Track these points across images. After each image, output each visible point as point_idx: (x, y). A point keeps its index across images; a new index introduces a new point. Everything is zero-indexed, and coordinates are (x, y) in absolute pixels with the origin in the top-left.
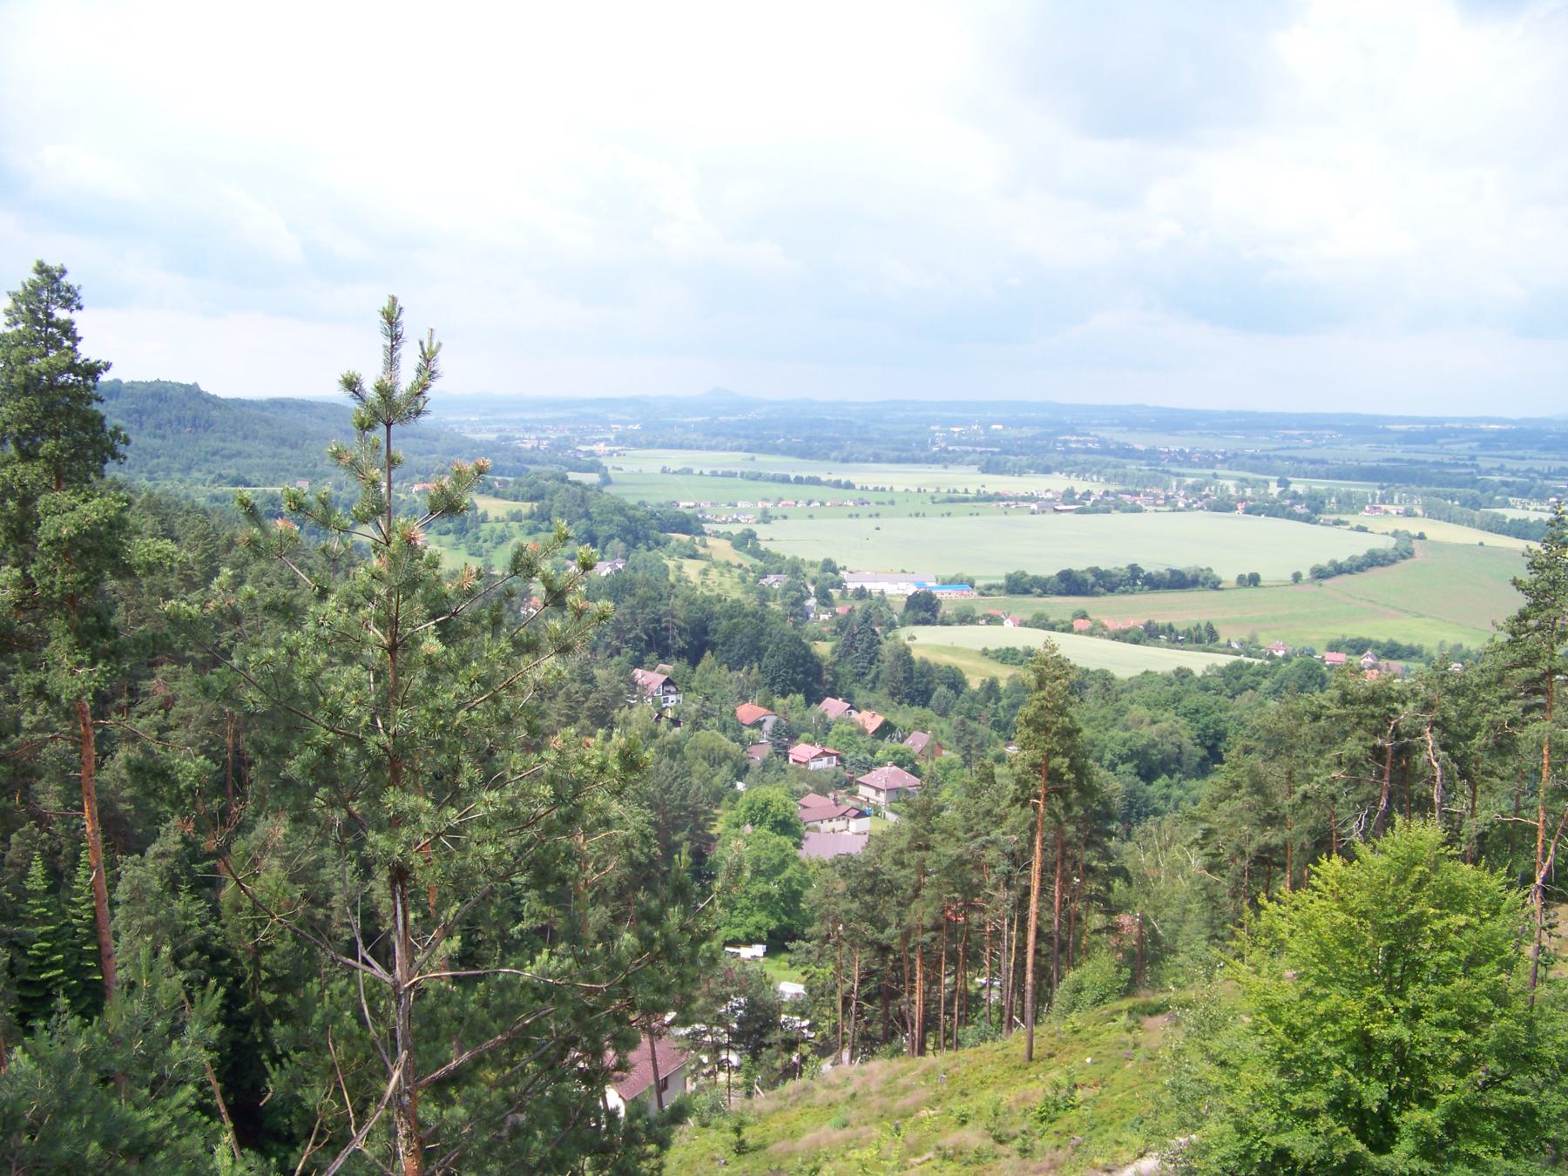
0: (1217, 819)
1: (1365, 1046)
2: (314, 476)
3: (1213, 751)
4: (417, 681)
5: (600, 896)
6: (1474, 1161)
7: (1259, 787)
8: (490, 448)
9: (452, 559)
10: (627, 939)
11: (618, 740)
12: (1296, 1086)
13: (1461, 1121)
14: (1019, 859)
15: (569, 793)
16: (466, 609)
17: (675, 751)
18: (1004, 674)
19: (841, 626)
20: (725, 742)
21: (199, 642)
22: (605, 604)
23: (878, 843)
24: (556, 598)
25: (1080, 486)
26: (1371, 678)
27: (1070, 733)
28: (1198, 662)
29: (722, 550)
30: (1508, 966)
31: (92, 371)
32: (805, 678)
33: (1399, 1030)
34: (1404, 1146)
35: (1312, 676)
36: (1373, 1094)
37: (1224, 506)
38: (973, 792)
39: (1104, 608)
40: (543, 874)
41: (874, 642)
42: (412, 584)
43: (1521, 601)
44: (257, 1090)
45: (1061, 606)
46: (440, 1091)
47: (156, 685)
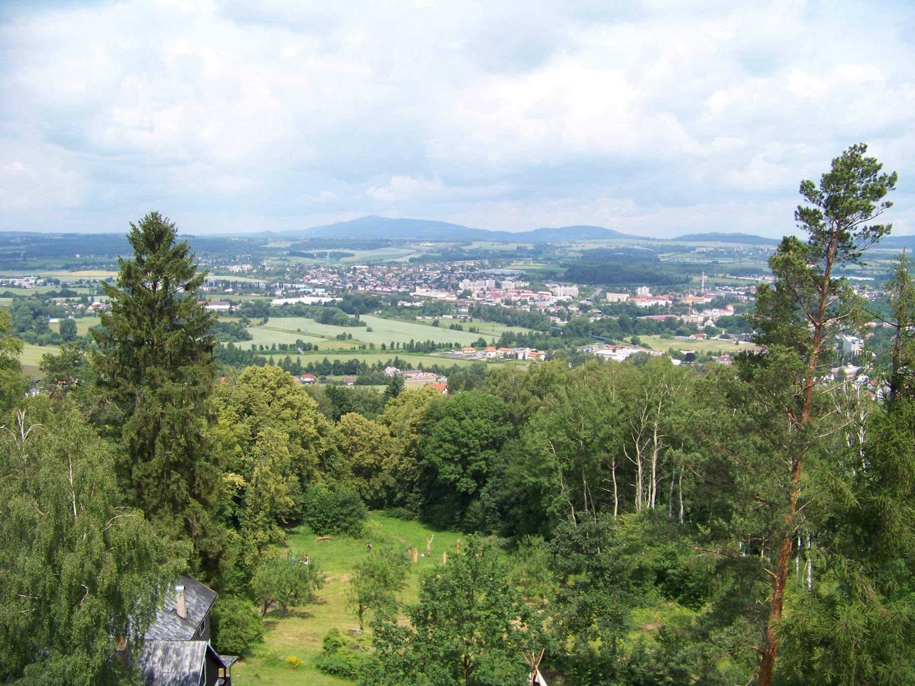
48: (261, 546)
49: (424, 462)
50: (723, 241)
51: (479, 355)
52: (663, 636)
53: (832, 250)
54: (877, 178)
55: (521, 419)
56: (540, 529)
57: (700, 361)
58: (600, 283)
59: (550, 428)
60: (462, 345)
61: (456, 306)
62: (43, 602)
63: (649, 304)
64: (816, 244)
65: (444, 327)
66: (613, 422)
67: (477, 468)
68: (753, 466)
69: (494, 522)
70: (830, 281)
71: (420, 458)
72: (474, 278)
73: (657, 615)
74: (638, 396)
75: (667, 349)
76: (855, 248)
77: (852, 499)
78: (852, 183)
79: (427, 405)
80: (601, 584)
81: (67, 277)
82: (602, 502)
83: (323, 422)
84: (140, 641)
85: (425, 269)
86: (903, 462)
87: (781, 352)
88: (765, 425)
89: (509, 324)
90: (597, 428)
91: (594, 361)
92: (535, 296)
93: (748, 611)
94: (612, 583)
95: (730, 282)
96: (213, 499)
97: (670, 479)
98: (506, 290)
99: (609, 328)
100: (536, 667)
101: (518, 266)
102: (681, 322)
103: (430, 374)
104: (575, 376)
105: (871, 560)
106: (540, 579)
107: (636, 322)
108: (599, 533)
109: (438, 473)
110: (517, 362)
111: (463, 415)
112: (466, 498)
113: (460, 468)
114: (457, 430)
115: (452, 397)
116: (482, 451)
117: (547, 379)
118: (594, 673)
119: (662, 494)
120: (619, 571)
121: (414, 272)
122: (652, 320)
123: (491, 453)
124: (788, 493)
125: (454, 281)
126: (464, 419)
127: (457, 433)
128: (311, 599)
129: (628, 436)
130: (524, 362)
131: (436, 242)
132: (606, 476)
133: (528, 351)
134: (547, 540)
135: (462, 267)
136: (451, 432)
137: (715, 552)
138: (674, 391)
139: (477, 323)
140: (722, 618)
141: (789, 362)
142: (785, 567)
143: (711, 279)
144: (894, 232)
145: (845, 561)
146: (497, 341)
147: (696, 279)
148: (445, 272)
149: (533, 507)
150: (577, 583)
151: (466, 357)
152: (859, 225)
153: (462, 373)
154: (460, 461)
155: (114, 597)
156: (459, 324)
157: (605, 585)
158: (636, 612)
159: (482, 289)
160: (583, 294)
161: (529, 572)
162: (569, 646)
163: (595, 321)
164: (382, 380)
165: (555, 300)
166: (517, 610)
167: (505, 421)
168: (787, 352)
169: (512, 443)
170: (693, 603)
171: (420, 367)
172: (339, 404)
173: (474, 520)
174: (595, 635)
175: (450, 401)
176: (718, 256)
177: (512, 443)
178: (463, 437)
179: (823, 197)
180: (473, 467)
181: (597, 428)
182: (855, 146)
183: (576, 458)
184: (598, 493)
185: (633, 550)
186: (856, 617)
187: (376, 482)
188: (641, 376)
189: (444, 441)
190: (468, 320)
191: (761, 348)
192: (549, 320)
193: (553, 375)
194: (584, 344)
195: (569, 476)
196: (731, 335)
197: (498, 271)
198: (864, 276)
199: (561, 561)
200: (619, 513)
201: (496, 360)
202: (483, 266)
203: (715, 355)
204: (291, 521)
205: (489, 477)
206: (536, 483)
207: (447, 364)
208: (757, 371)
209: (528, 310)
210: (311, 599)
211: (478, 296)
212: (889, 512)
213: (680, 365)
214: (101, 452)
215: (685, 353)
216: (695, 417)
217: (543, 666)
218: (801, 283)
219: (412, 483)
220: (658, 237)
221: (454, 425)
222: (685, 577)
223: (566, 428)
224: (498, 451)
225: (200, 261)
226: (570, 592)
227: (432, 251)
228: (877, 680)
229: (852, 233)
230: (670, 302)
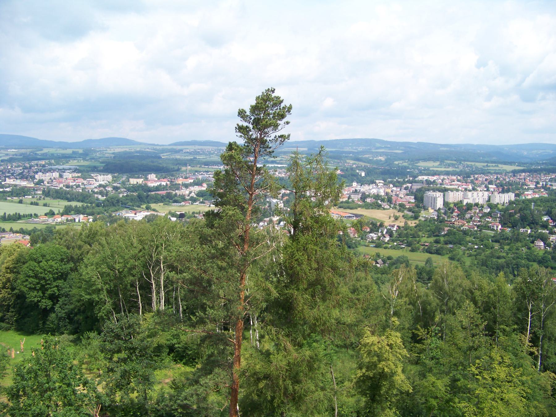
49: (16, 291)
50: (199, 145)
51: (50, 220)
52: (175, 385)
53: (257, 150)
54: (281, 107)
55: (79, 259)
56: (95, 327)
57: (188, 218)
58: (124, 173)
59: (97, 264)
60: (39, 215)
61: (34, 190)
63: (156, 184)
64: (248, 146)
65: (26, 203)
66: (135, 257)
67: (52, 293)
68: (217, 279)
69: (65, 326)
70: (257, 168)
71: (13, 289)
72: (45, 172)
73: (170, 373)
74: (150, 241)
75: (168, 212)
76: (270, 148)
77: (275, 294)
78: (267, 110)
79: (16, 254)
80: (134, 358)
82: (132, 307)
85: (12, 167)
86: (301, 270)
87: (230, 210)
88: (223, 254)
89: (69, 200)
90: (126, 262)
91: (123, 220)
92: (85, 182)
93: (221, 365)
94: (141, 356)
95: (204, 170)
97: (173, 290)
98: (66, 179)
99: (132, 200)
100: (97, 414)
101: (74, 163)
102: (176, 194)
103: (18, 235)
104: (111, 230)
105: (288, 328)
106: (97, 359)
107: (148, 196)
108: (130, 326)
109: (26, 298)
110: (75, 224)
111: (41, 259)
112: (46, 312)
113: (40, 293)
114: (37, 269)
115: (33, 248)
116: (54, 281)
117: (94, 233)
118: (134, 413)
119: (169, 299)
120: (145, 349)
121: (4, 169)
122: (158, 194)
123: (60, 282)
124: (238, 293)
125: (32, 174)
126: (41, 262)
127: (38, 271)
129: (145, 266)
130: (79, 224)
131: (18, 149)
132: (133, 291)
133: (82, 216)
134: (99, 334)
135: (37, 165)
136: (33, 271)
137: (199, 332)
138: (171, 237)
139: (48, 200)
140: (206, 370)
141: (234, 216)
142: (240, 337)
143: (193, 168)
144: (292, 139)
145: (274, 330)
146: (61, 211)
147: (184, 168)
148: (25, 168)
149: (89, 314)
150: (119, 358)
151: (42, 222)
152: (272, 135)
153: (39, 232)
154: (40, 289)
156: (36, 201)
157: (137, 358)
158: (157, 372)
159: (51, 179)
160: (115, 179)
161: (90, 356)
162: (118, 399)
163: (123, 196)
165: (97, 184)
166: (80, 379)
167: (68, 262)
168: (233, 210)
170: (192, 363)
171: (11, 230)
173: (52, 326)
174: (133, 390)
175: (31, 251)
176: (197, 154)
177: (73, 275)
178: (41, 273)
179: (251, 119)
180: (49, 292)
181: (126, 262)
182: (268, 89)
183: (114, 282)
184: (129, 302)
185: (153, 335)
186: (281, 361)
188: (152, 229)
189: (29, 277)
190: (42, 199)
191: (218, 209)
192: (94, 196)
193: (97, 231)
194: (117, 211)
195: (111, 293)
196: (206, 201)
197: (61, 167)
198: (281, 164)
199: (108, 346)
200: (143, 313)
201: (61, 223)
202: (50, 164)
203: (197, 214)
205: (60, 298)
206: (90, 299)
207: (30, 227)
208: (216, 222)
209: (81, 191)
211: (48, 183)
212: (296, 299)
213: (176, 221)
215: (179, 213)
216: (181, 252)
217: (102, 413)
218: (240, 169)
219: (9, 306)
220: (160, 144)
221: (35, 266)
222: (186, 348)
223: (107, 263)
224: (65, 280)
226: (115, 364)
227: (16, 155)
228: (295, 394)
229: (268, 139)
230: (169, 183)
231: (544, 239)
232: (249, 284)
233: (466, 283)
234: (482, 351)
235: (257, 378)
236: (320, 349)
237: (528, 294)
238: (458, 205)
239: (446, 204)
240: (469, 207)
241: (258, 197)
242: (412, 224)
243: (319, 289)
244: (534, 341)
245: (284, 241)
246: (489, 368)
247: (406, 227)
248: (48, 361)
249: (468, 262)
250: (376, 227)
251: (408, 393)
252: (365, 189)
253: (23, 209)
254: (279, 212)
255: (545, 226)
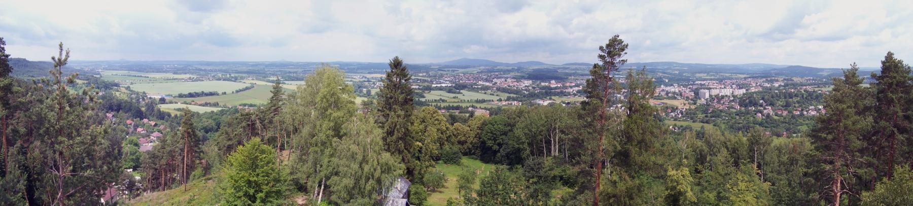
0: (219, 140)
1: (249, 182)
2: (46, 76)
3: (218, 125)
4: (65, 115)
5: (100, 159)
6: (271, 202)
7: (227, 133)
8: (79, 71)
9: (72, 92)
10: (105, 167)
11: (103, 127)
12: (237, 192)
13: (268, 195)
14: (182, 150)
15: (94, 138)
16: (74, 101)
17: (114, 130)
18: (178, 113)
19: (147, 104)
20: (124, 128)
21: (25, 107)
22: (101, 101)
23: (155, 147)
24: (91, 99)
25: (192, 76)
26: (247, 111)
27: (192, 124)
28: (215, 109)
29: (123, 90)
30: (273, 163)
31: (7, 56)
32: (140, 115)
33: (255, 178)
34: (258, 201)
35: (237, 111)
36: (252, 191)
37: (219, 79)
38: (173, 137)
39: (197, 100)
40: (89, 154)
41: (153, 108)
42: (64, 96)
43: (272, 95)
44: (33, 195)
45: (189, 100)
46: (68, 197)
47: (17, 115)
48: (427, 167)
52: (563, 199)
62: (357, 180)
66: (543, 125)
73: (560, 192)
77: (619, 148)
81: (369, 76)
82: (541, 153)
83: (448, 125)
84: (386, 197)
90: (538, 128)
96: (411, 150)
101: (512, 74)
112: (495, 152)
123: (504, 137)
128: (443, 186)
137: (577, 169)
139: (499, 93)
144: (628, 62)
151: (495, 104)
152: (618, 60)
155: (379, 181)
158: (553, 191)
164: (468, 112)
169: (509, 134)
172: (453, 119)
187: (465, 146)
199: (527, 174)
204: (437, 159)
207: (489, 107)
208: (587, 107)
210: (443, 186)
214: (379, 133)
225: (410, 72)
231: (761, 112)
232: (605, 142)
233: (722, 138)
234: (732, 175)
235: (609, 196)
236: (644, 179)
237: (754, 142)
238: (717, 96)
239: (710, 96)
240: (723, 97)
241: (610, 93)
242: (693, 107)
243: (643, 145)
244: (759, 167)
245: (624, 118)
246: (737, 184)
247: (690, 109)
248: (497, 179)
249: (723, 126)
250: (674, 109)
251: (695, 203)
252: (668, 89)
253: (486, 97)
254: (621, 102)
255: (761, 106)
